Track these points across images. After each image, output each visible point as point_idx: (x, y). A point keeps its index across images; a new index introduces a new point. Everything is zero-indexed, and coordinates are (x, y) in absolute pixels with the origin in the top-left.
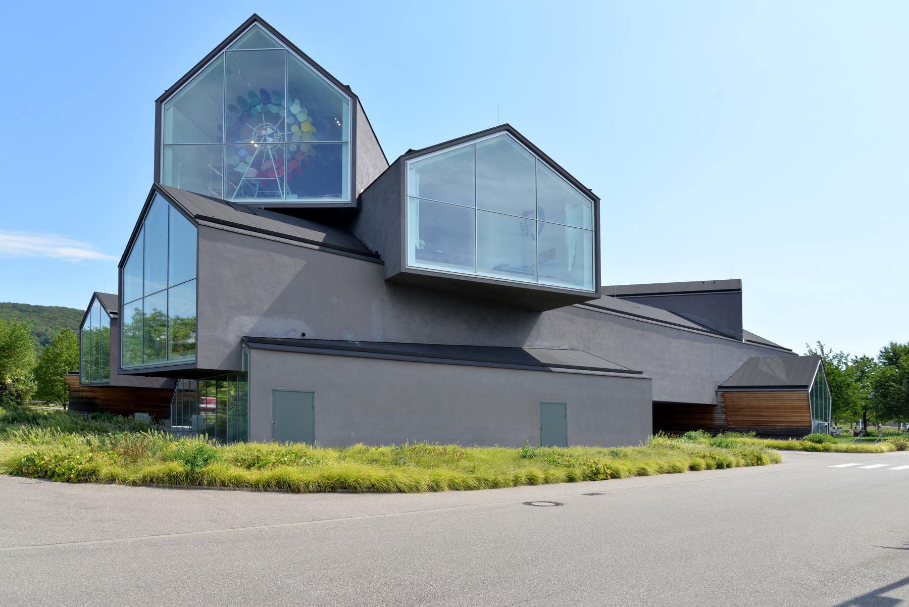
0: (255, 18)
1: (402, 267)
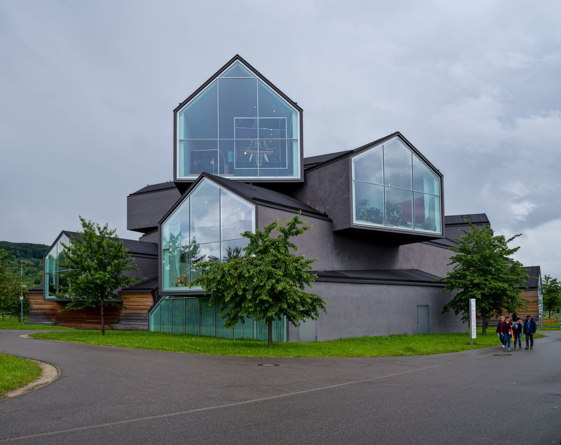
0: (237, 57)
1: (351, 224)
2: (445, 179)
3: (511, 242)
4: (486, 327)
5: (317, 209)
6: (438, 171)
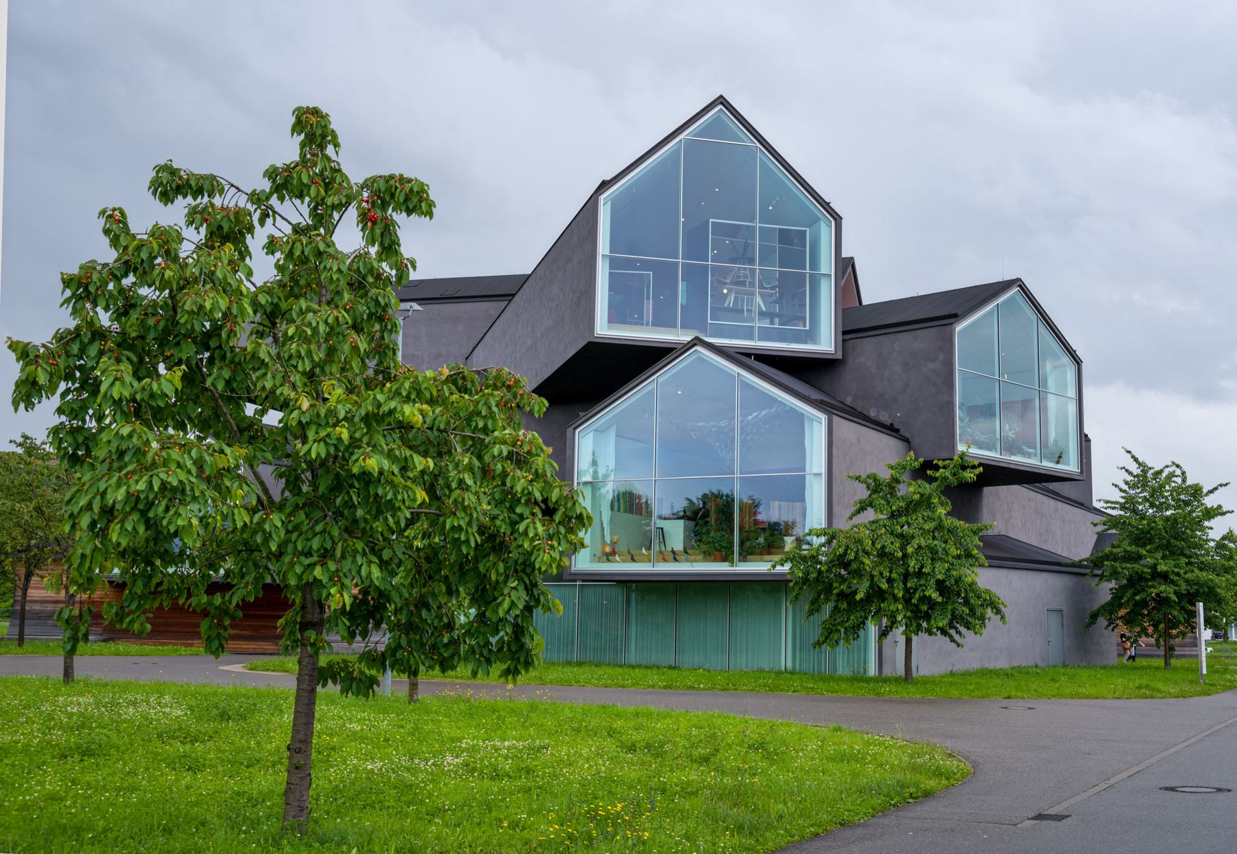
0: (721, 100)
3: (1211, 495)
4: (1171, 656)
5: (872, 415)
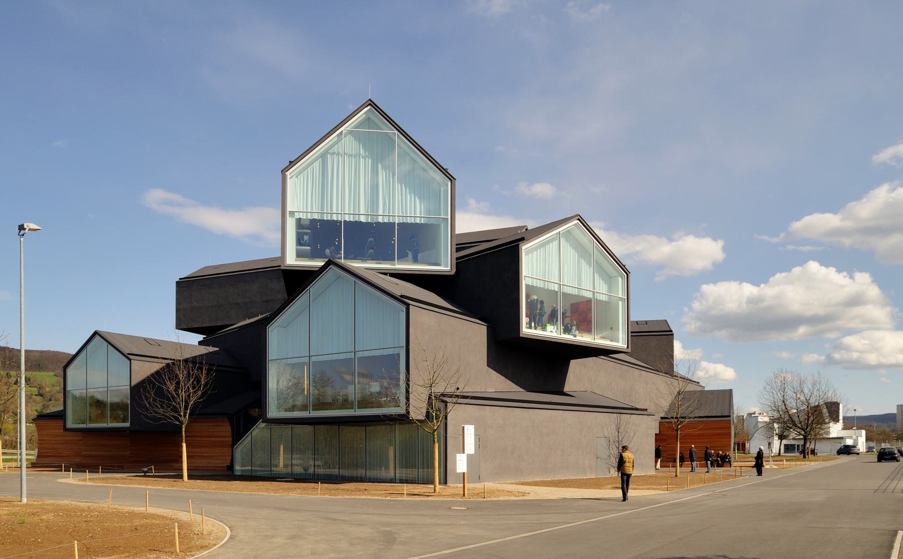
2: (631, 276)
6: (624, 266)
